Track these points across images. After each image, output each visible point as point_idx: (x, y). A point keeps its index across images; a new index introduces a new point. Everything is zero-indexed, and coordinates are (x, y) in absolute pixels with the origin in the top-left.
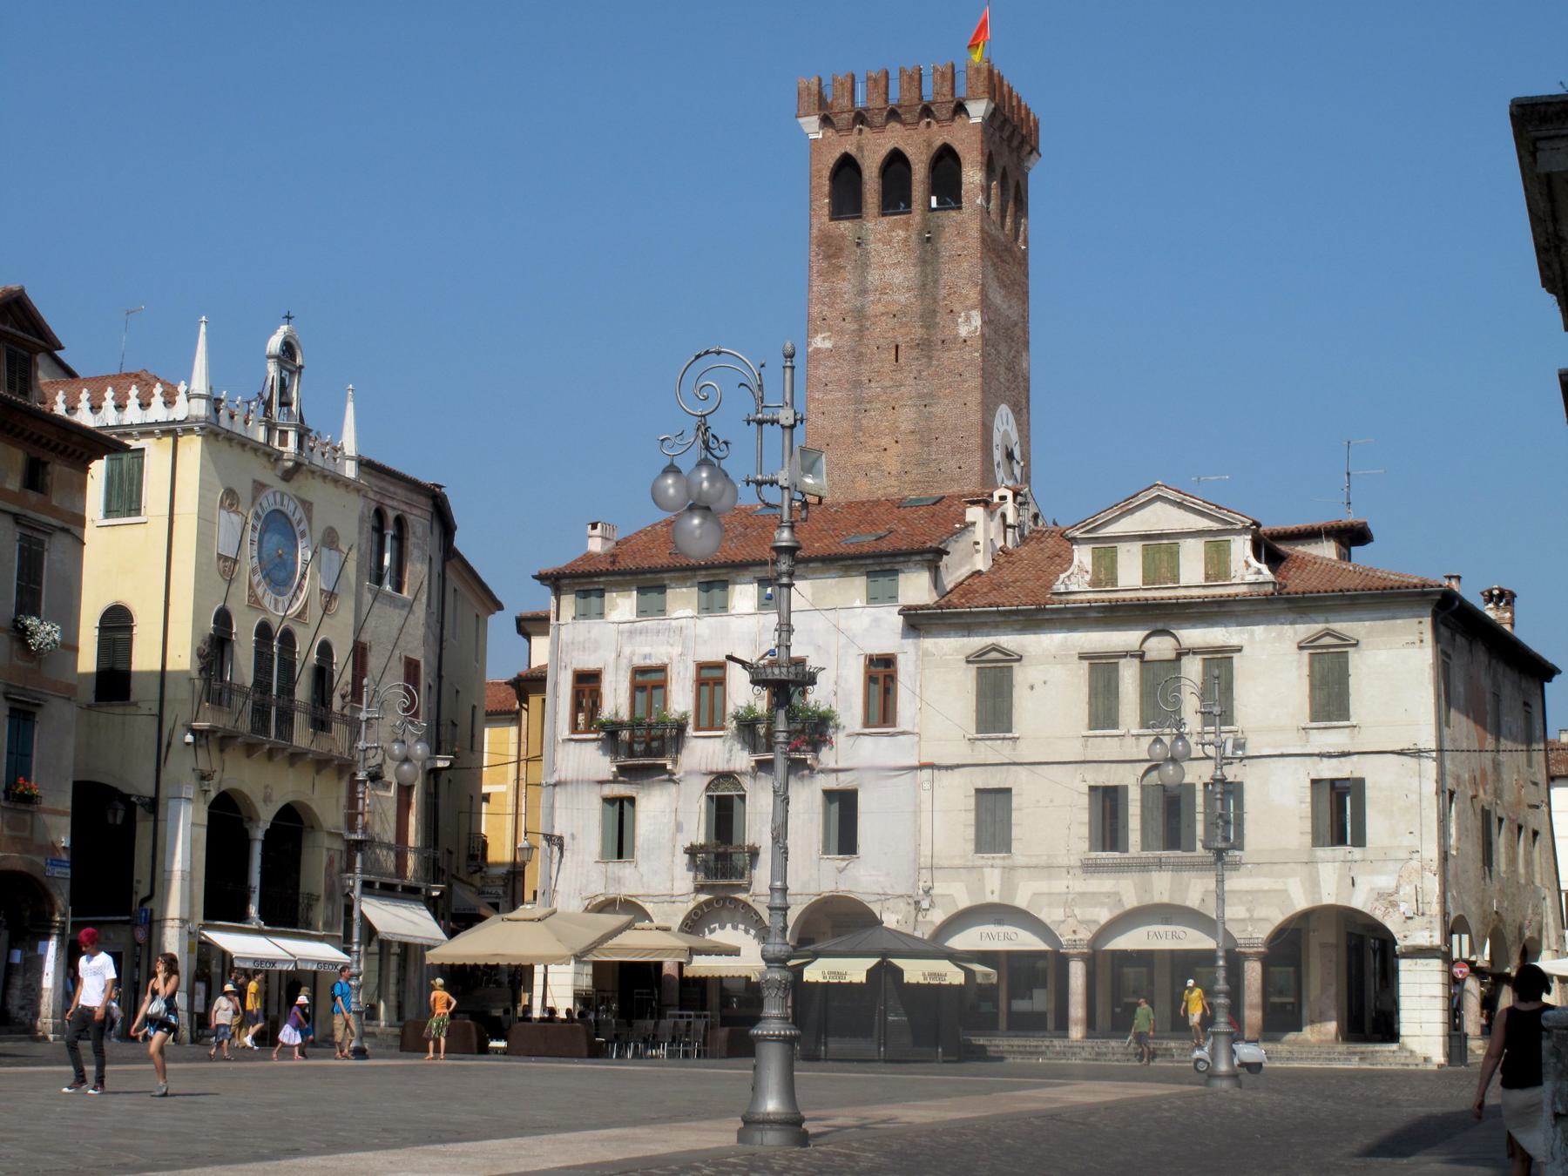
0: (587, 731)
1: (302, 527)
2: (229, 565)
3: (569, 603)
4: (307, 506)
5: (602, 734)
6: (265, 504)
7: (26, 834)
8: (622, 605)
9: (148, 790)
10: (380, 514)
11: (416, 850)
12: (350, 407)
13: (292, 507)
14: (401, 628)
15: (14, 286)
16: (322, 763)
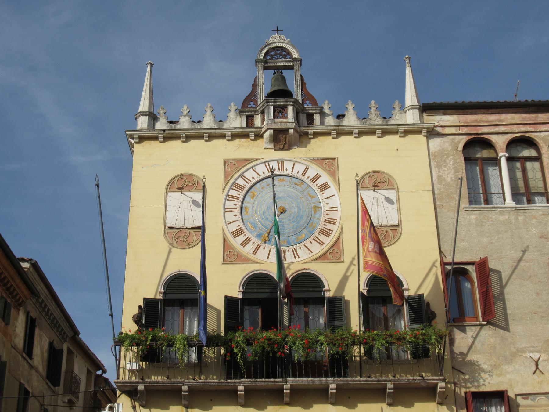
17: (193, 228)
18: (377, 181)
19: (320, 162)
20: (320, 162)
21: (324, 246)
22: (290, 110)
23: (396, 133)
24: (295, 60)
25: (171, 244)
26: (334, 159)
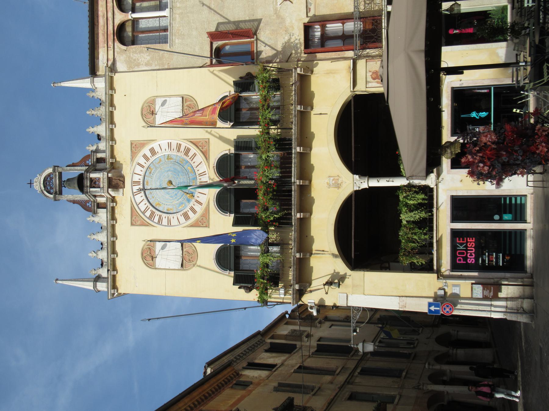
17: (182, 249)
18: (149, 112)
19: (133, 154)
20: (133, 154)
21: (197, 153)
22: (93, 175)
23: (112, 95)
24: (54, 171)
25: (194, 265)
26: (132, 144)
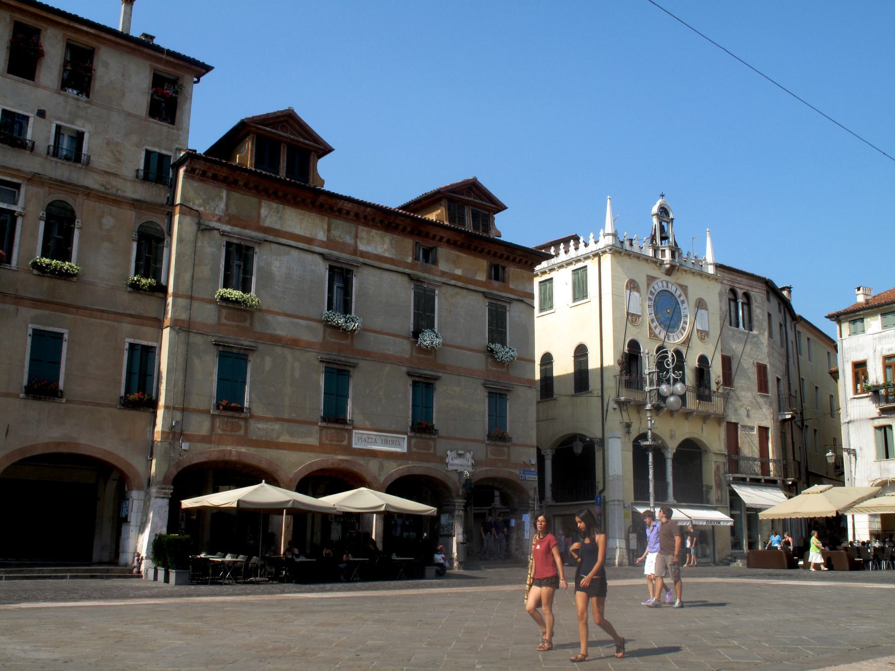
0: (863, 392)
1: (682, 298)
2: (633, 318)
3: (846, 326)
4: (684, 288)
5: (870, 393)
6: (656, 287)
7: (505, 457)
8: (874, 324)
9: (599, 435)
10: (733, 291)
11: (774, 461)
12: (708, 239)
13: (674, 288)
14: (757, 349)
15: (470, 176)
16: (705, 418)
20: (681, 286)
